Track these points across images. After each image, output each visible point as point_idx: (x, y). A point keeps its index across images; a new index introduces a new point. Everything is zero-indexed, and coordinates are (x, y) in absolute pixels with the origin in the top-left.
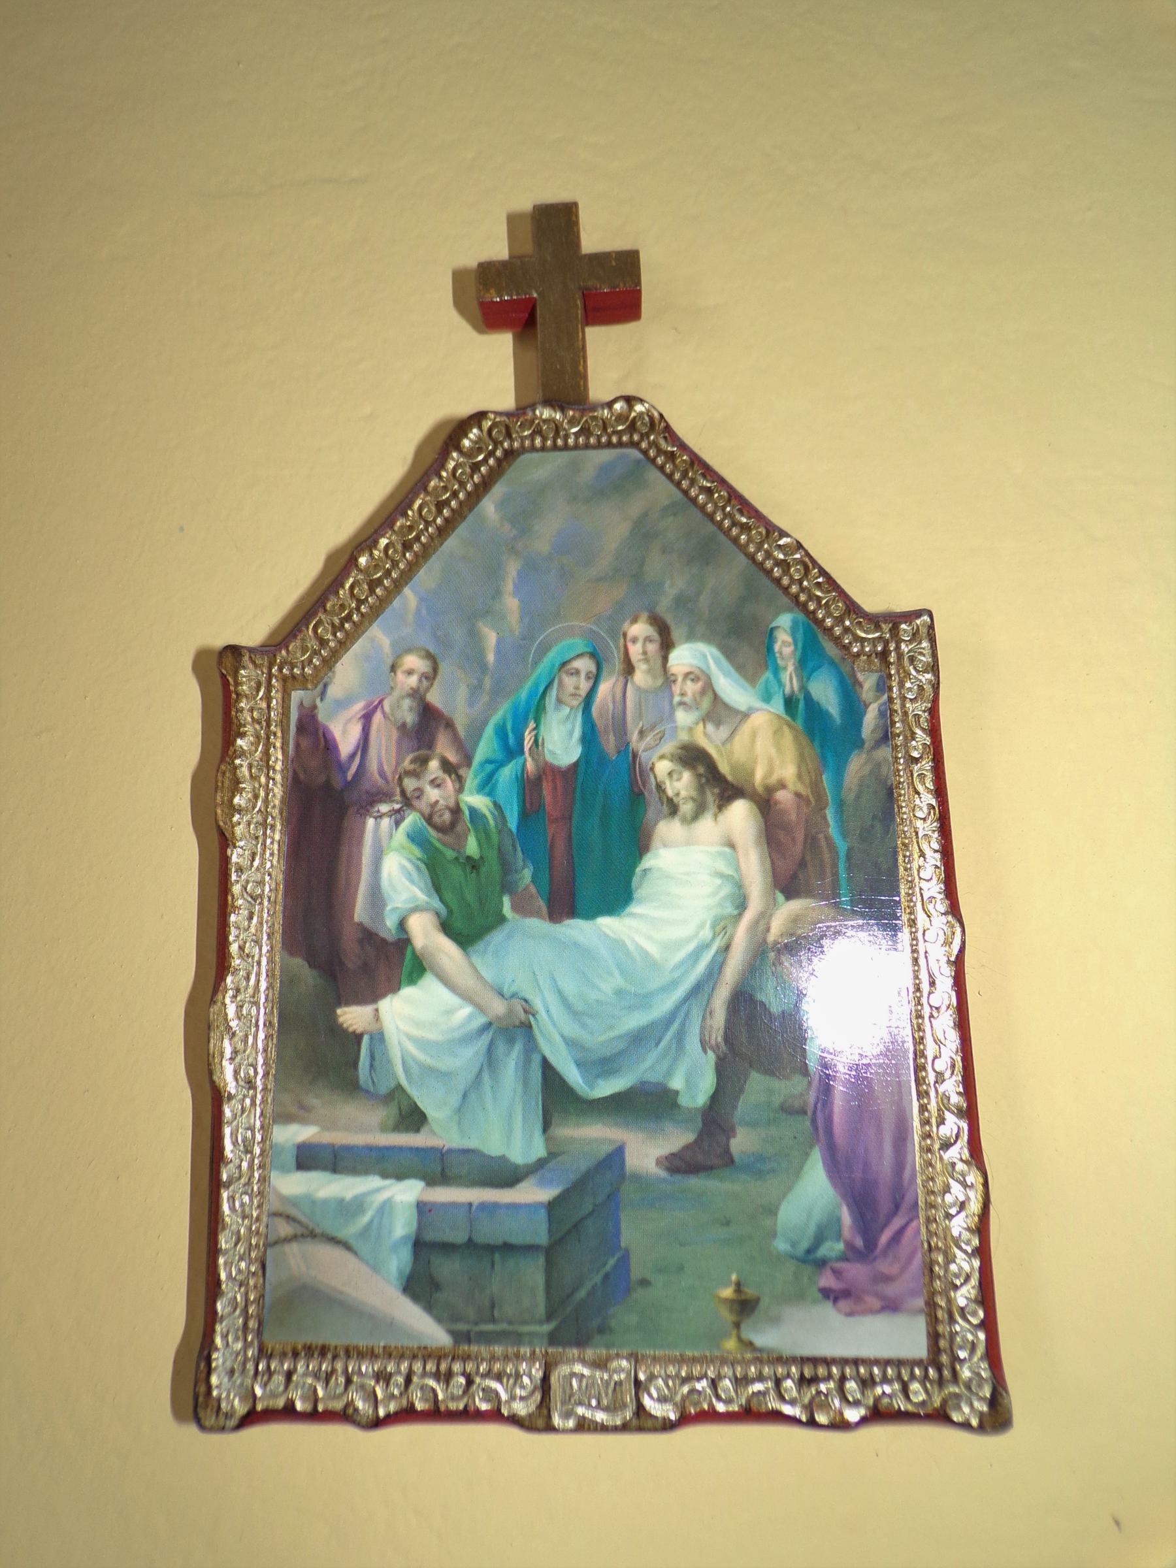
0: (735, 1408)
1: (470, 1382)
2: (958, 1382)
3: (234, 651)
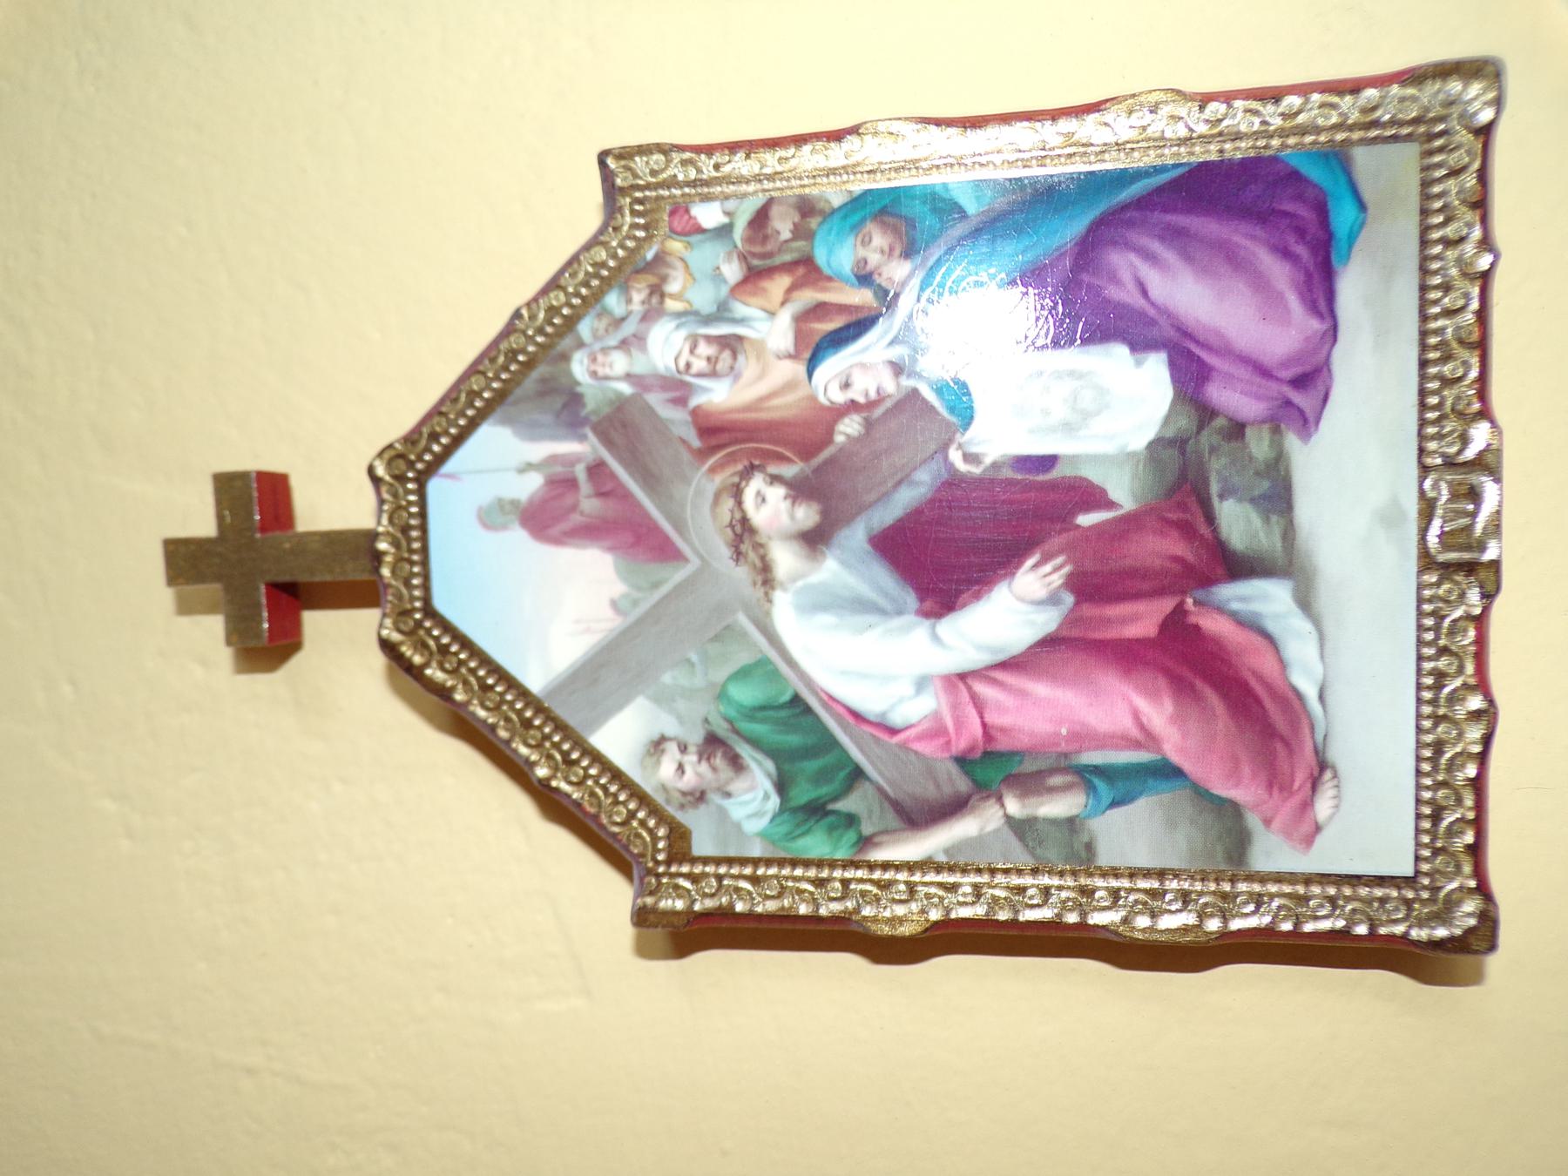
0: (1475, 361)
1: (1444, 651)
2: (1443, 120)
3: (642, 917)
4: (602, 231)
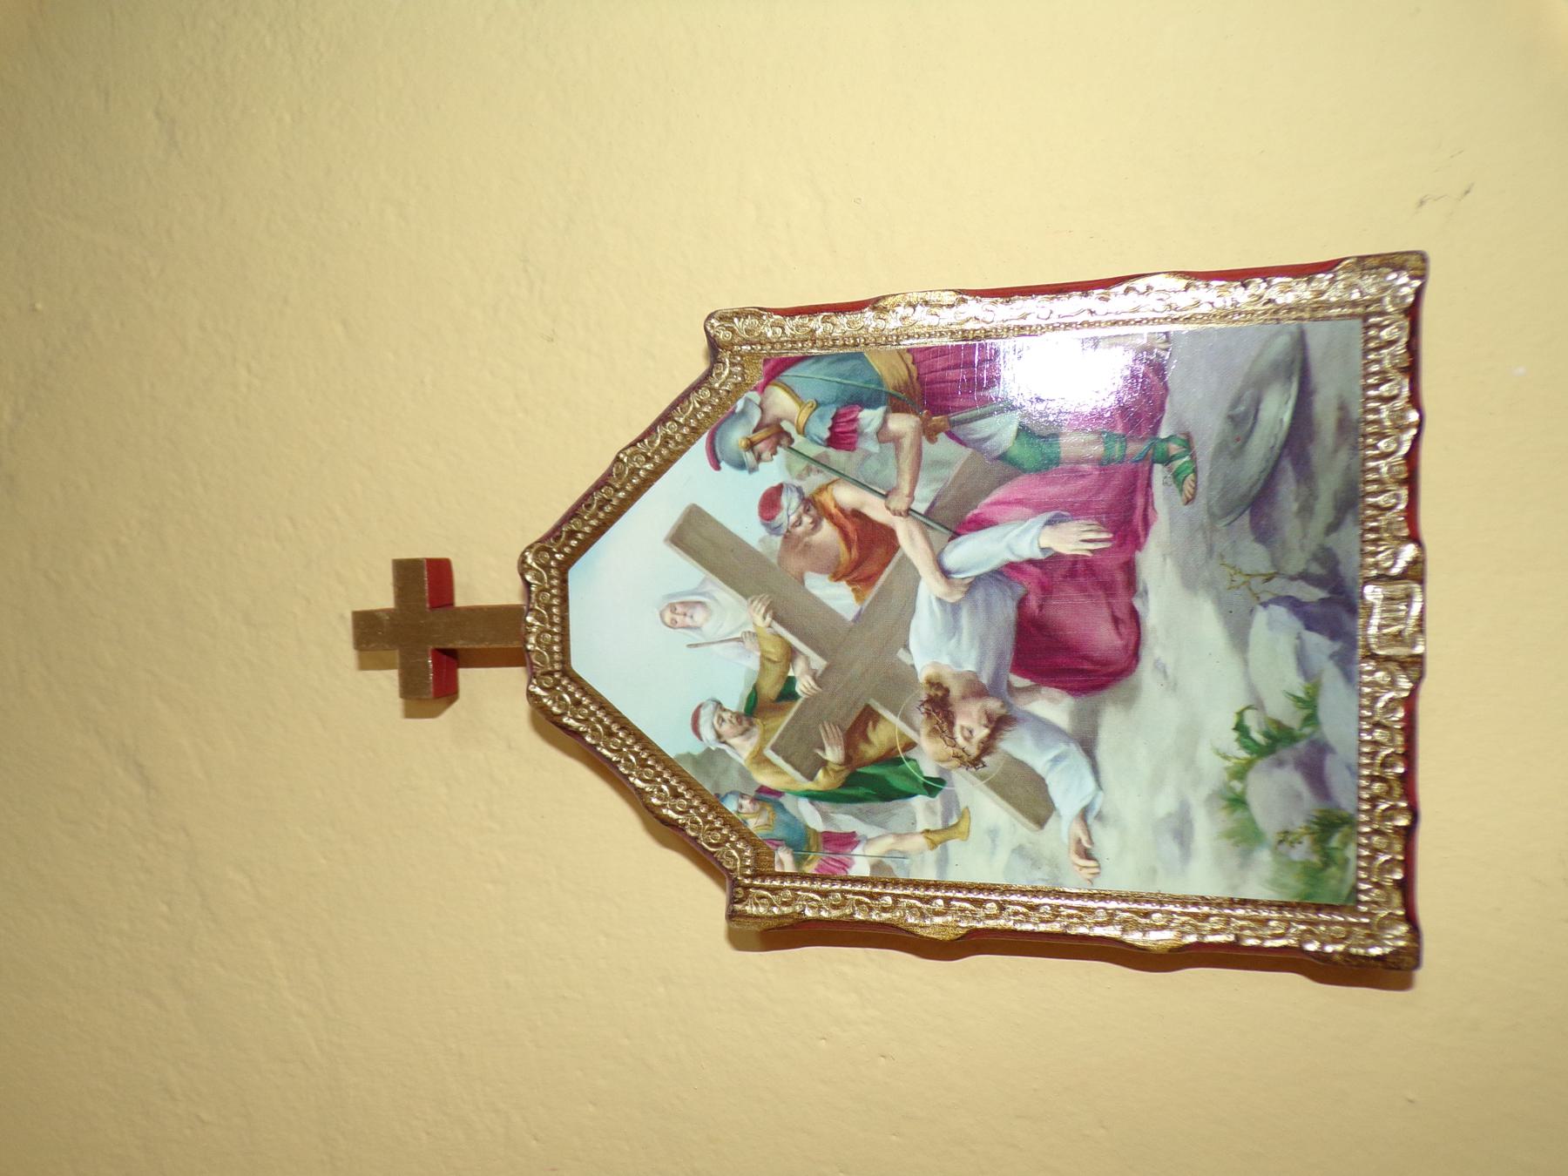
0: (1404, 492)
1: (1378, 725)
4: (708, 374)
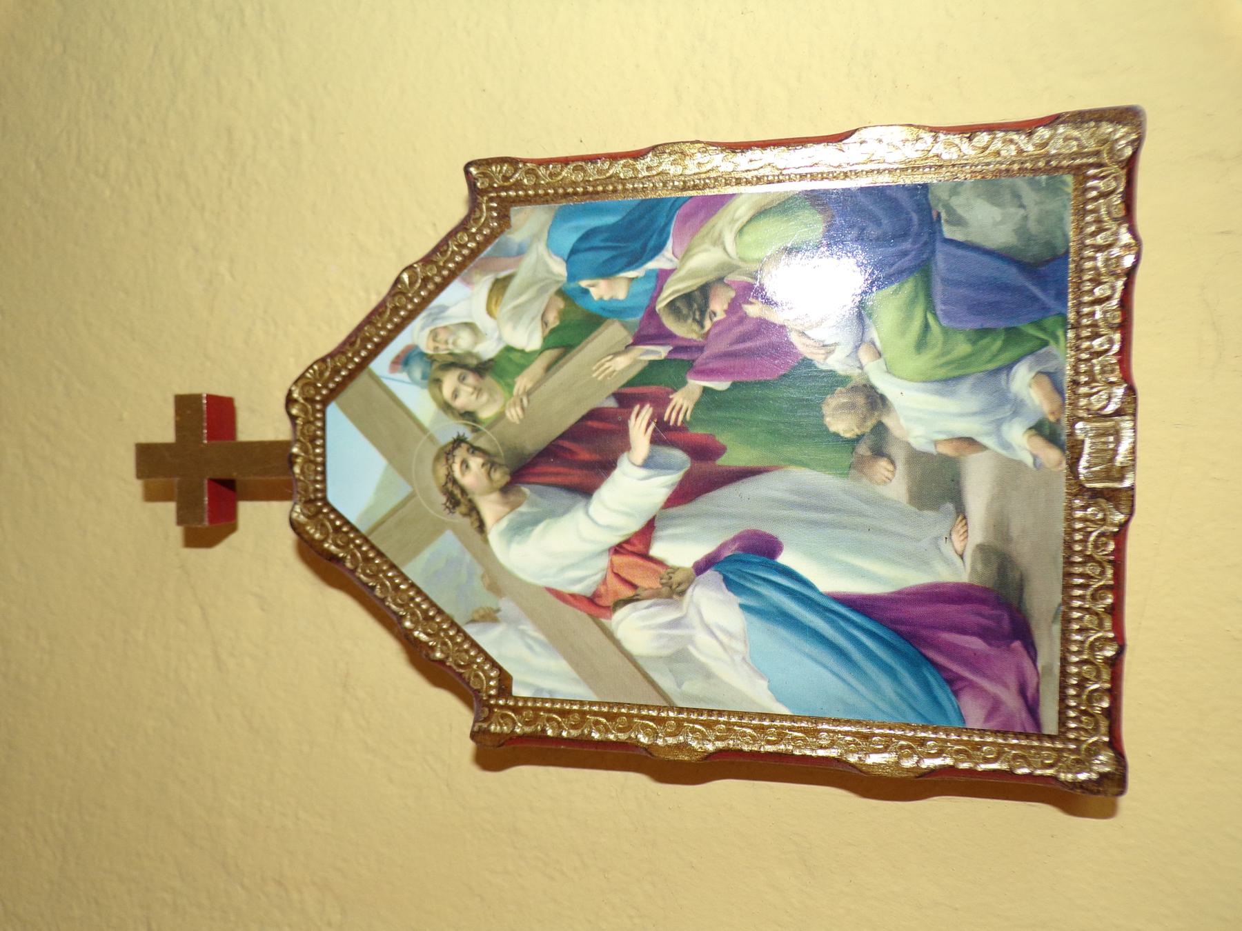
0: (1117, 336)
2: (1099, 158)
